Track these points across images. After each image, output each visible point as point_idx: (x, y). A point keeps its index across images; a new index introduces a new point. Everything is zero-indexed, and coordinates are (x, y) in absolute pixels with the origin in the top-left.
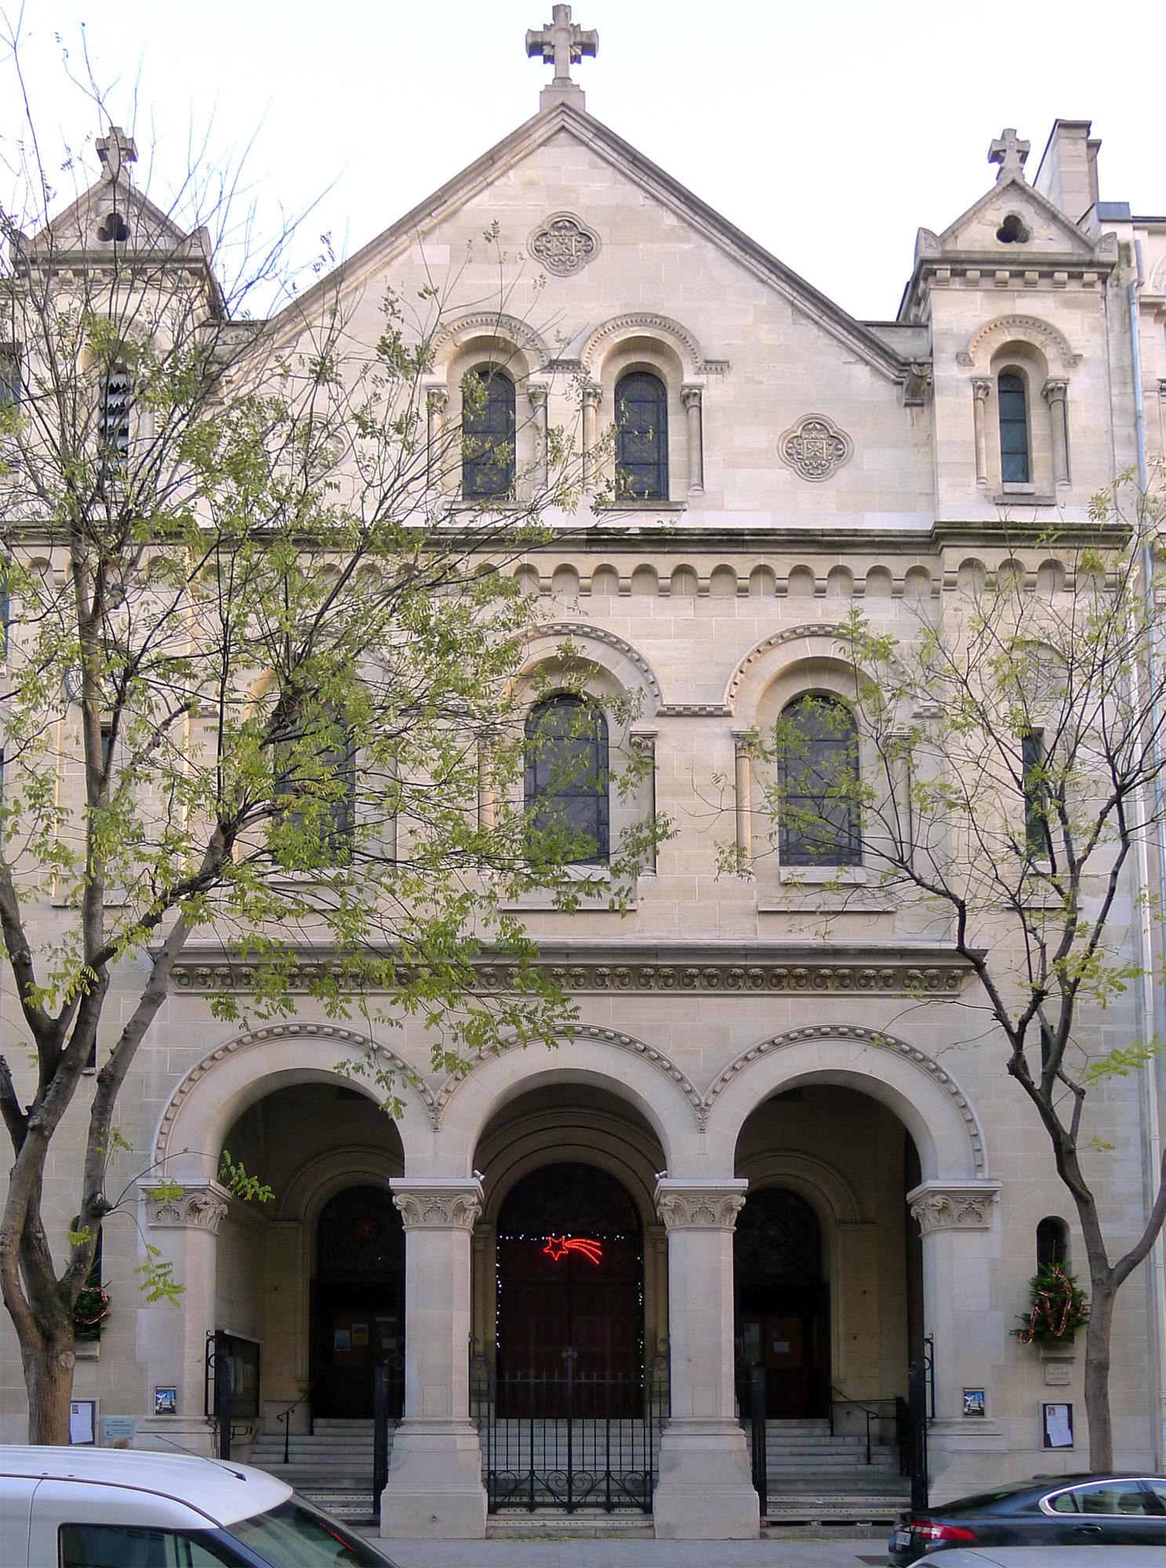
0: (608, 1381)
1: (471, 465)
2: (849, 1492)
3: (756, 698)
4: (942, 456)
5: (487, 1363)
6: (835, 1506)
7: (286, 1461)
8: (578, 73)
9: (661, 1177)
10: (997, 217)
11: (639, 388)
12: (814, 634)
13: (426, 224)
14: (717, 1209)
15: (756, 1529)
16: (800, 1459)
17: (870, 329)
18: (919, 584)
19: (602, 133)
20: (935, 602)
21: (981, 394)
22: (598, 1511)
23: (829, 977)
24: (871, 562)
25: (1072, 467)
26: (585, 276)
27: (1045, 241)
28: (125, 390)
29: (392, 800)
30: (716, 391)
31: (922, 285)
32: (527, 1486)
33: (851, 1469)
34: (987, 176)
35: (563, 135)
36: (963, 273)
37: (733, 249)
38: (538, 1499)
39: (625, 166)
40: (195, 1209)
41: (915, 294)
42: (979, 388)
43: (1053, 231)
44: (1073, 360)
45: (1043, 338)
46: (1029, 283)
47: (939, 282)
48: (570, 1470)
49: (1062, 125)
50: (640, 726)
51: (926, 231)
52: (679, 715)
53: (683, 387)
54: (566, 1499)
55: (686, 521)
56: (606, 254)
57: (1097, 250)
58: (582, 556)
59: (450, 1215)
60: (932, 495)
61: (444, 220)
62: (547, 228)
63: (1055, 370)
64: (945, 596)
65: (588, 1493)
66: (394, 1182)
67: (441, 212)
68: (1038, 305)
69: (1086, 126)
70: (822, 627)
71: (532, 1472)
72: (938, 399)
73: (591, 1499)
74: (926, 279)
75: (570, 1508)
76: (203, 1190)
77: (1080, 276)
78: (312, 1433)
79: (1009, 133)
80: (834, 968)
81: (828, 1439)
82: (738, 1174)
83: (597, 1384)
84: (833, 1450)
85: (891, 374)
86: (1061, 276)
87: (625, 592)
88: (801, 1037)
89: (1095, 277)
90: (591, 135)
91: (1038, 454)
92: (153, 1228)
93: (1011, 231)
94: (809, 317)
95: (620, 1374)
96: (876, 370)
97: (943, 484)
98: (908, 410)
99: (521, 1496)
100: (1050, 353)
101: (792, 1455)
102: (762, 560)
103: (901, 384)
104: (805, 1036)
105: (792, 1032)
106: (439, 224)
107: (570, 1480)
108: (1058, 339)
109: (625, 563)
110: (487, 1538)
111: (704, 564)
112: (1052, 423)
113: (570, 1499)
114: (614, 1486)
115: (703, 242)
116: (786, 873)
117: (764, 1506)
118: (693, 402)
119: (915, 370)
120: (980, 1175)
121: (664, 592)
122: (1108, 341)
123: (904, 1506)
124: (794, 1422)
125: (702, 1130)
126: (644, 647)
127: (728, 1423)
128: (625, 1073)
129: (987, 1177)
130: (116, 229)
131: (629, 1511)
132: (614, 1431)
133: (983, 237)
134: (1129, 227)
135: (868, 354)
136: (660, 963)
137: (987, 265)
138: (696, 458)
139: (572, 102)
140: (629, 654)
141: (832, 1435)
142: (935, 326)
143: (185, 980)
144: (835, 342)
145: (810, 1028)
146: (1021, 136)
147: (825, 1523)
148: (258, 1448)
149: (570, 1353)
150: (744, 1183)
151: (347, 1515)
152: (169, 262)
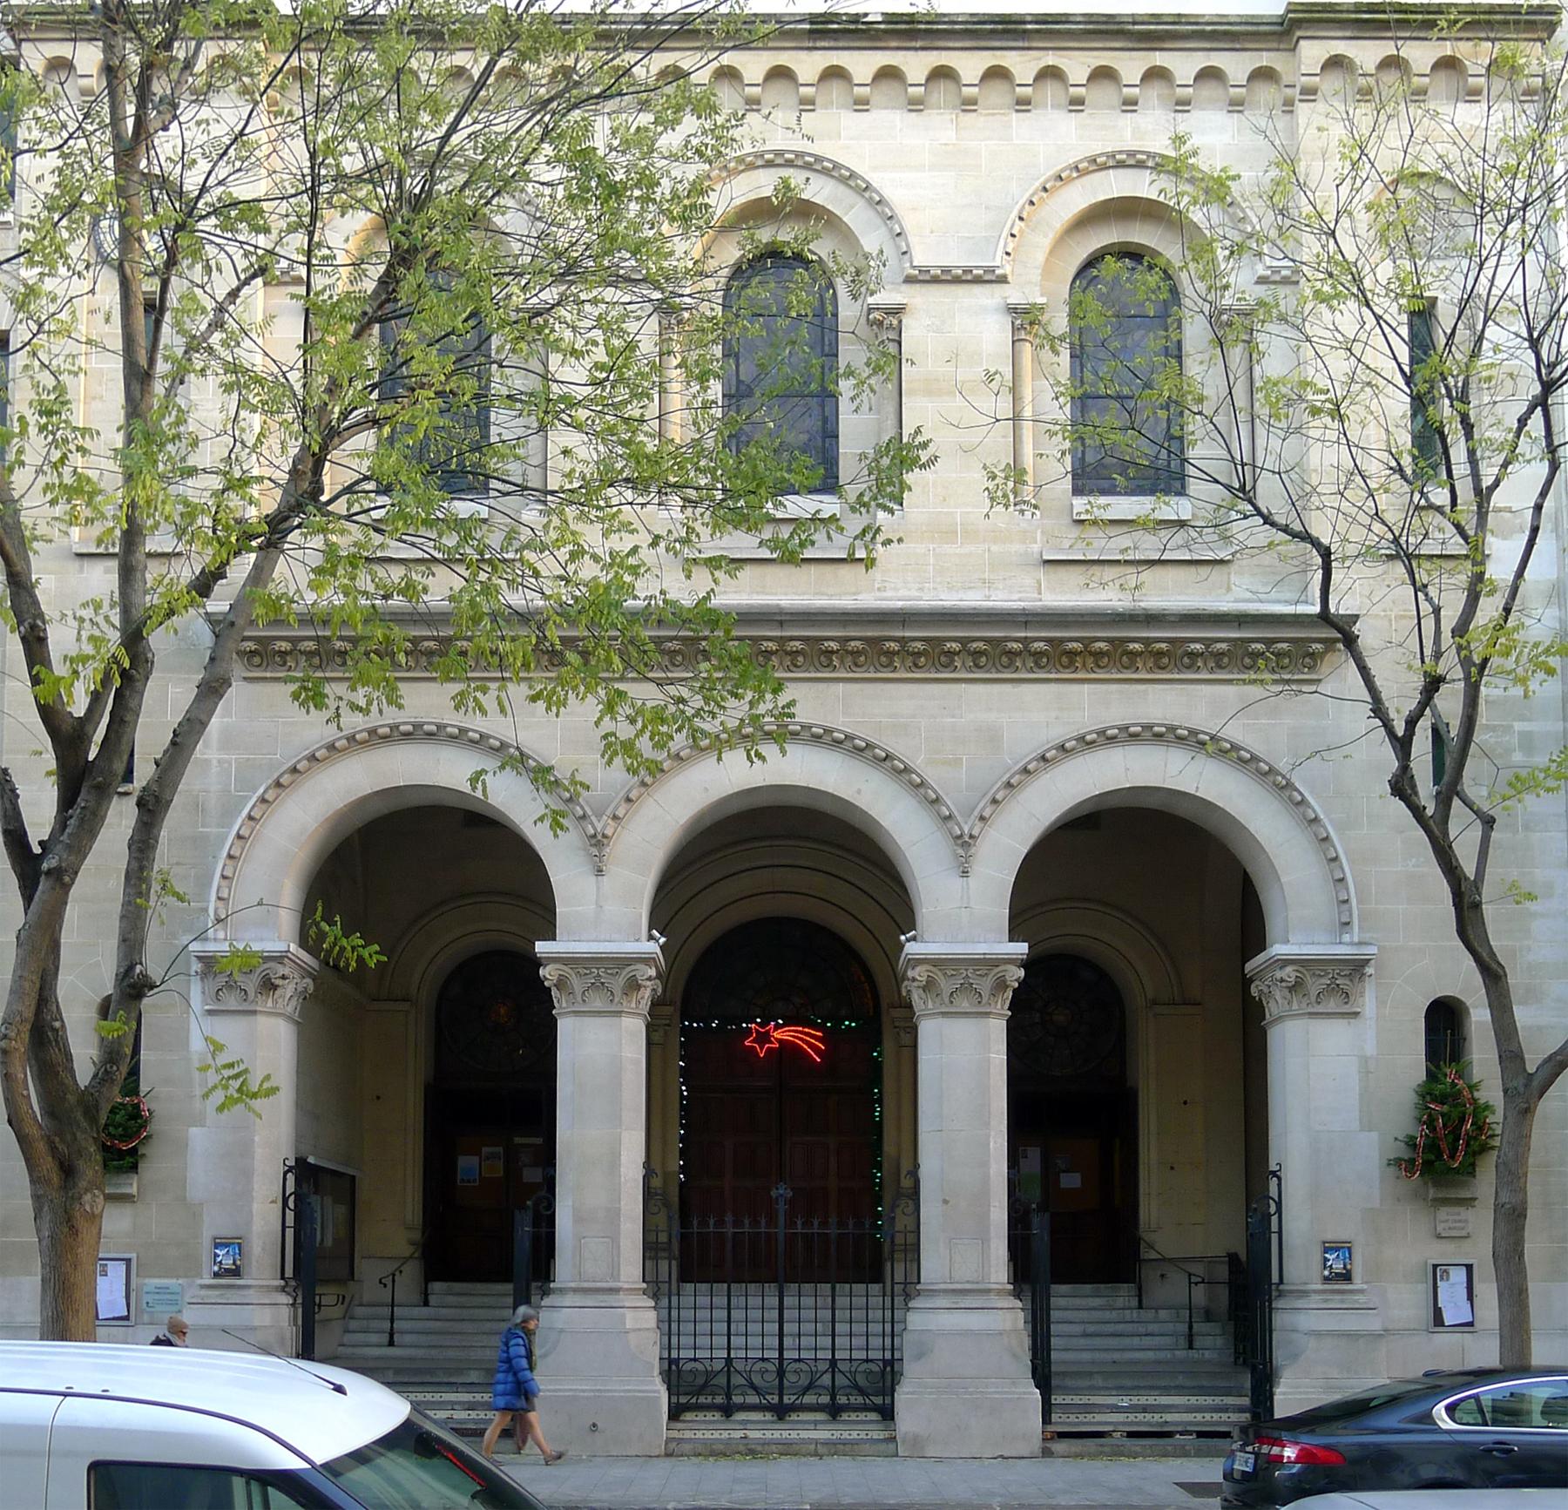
2: (1166, 1390)
3: (1040, 256)
5: (666, 1204)
6: (1145, 1409)
7: (391, 1343)
9: (908, 940)
14: (985, 985)
15: (1036, 1443)
18: (1266, 93)
24: (1200, 60)
32: (722, 1380)
38: (737, 1399)
40: (269, 986)
52: (935, 280)
54: (776, 1399)
58: (803, 55)
59: (618, 992)
64: (1303, 109)
65: (805, 1390)
66: (541, 947)
70: (1132, 154)
73: (809, 1399)
75: (781, 1412)
76: (280, 959)
78: (426, 1304)
80: (1147, 642)
84: (1142, 1329)
87: (861, 104)
92: (210, 1012)
99: (714, 1394)
101: (1085, 1335)
102: (1051, 59)
105: (1090, 733)
107: (781, 1373)
109: (862, 64)
113: (781, 1399)
120: (1346, 938)
121: (916, 105)
123: (1241, 1410)
126: (884, 183)
127: (999, 1292)
128: (859, 792)
129: (1356, 939)
132: (842, 1301)
140: (867, 195)
141: (1140, 1307)
143: (257, 660)
147: (1131, 1435)
148: (353, 1324)
149: (781, 1191)
150: (1022, 948)
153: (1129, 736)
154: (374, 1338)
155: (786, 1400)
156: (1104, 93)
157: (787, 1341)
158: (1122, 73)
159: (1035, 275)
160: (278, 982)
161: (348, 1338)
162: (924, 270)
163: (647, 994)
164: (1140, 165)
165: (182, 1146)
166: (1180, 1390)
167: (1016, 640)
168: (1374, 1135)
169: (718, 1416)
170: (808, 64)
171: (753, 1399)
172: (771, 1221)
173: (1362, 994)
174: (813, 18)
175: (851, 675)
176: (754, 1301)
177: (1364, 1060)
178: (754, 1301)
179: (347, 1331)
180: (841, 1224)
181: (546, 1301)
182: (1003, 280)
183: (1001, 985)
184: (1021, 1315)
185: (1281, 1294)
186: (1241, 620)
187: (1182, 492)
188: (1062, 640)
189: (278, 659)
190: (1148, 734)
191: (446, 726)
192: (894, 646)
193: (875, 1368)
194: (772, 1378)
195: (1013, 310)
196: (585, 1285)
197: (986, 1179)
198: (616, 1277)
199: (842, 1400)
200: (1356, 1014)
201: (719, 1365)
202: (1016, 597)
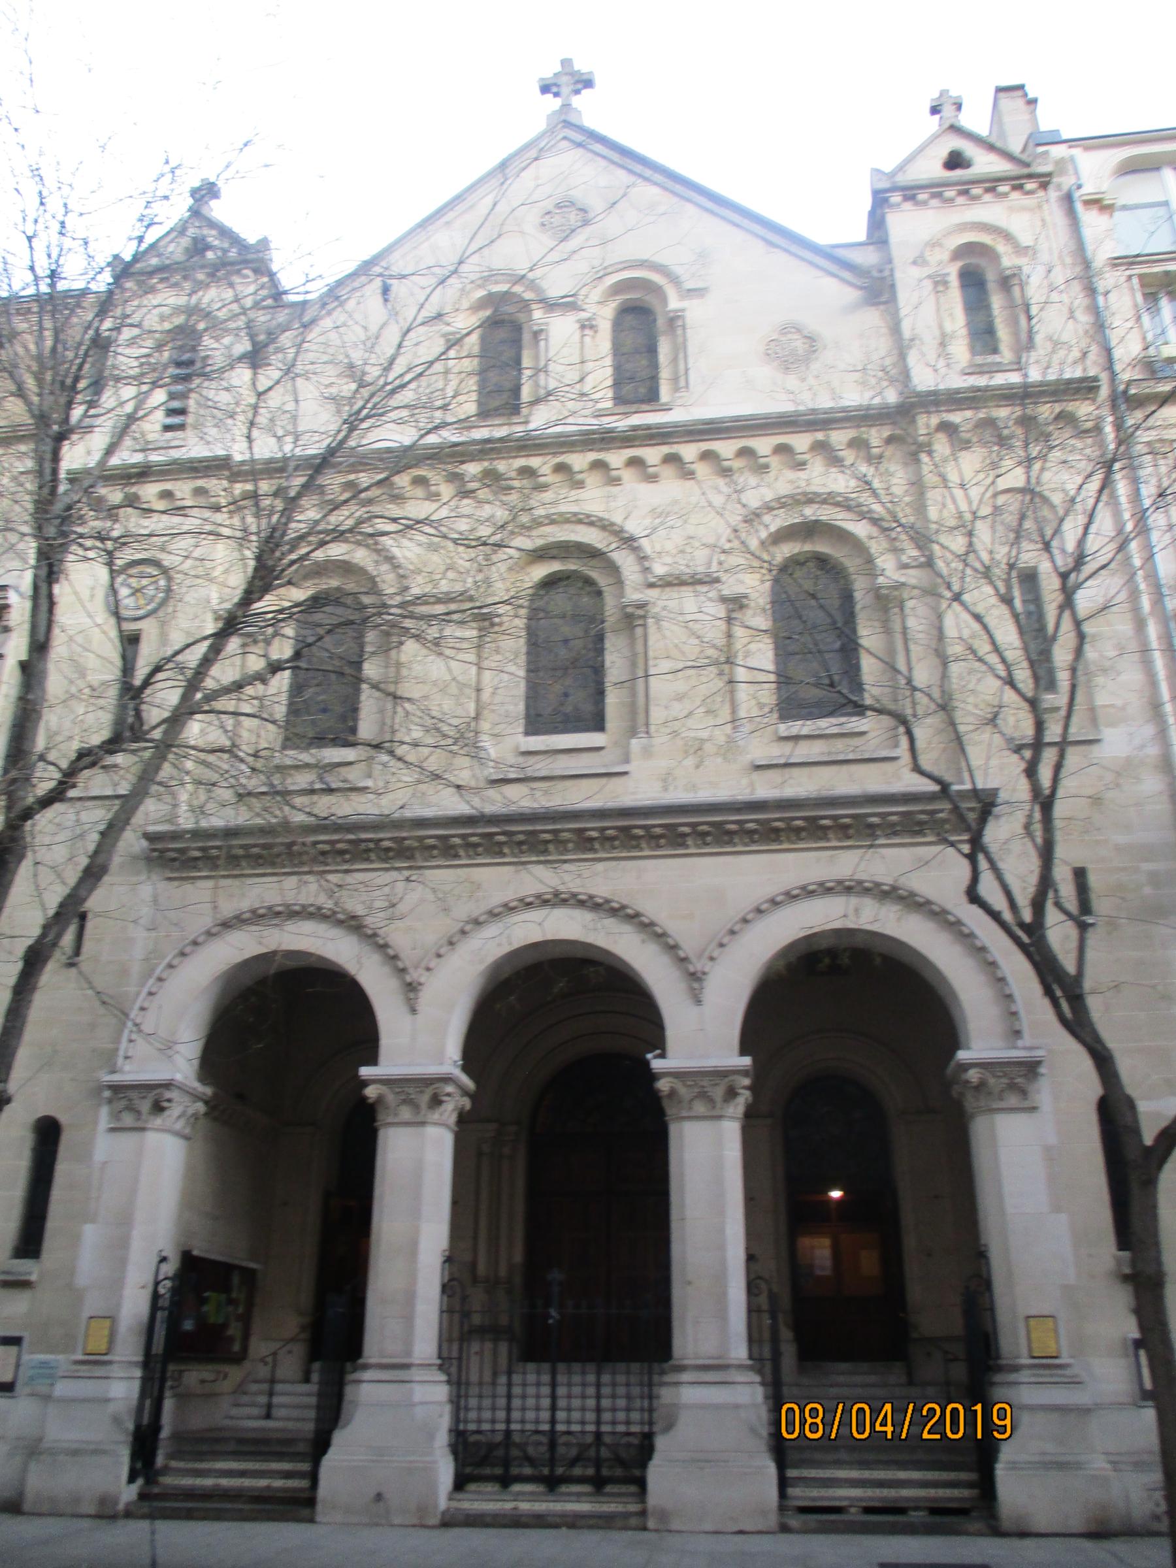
6: (881, 1484)
7: (268, 1416)
10: (942, 151)
11: (502, 334)
13: (450, 216)
15: (772, 1520)
22: (586, 1488)
23: (878, 825)
24: (592, 456)
27: (985, 163)
30: (695, 312)
31: (879, 212)
34: (933, 124)
37: (710, 205)
38: (515, 1471)
39: (615, 156)
41: (877, 223)
43: (992, 157)
46: (976, 198)
47: (891, 206)
49: (1000, 90)
51: (878, 170)
54: (546, 1471)
55: (676, 416)
65: (573, 1463)
66: (365, 1071)
67: (460, 208)
68: (990, 211)
69: (1021, 87)
73: (577, 1471)
76: (447, 1079)
79: (943, 93)
80: (835, 818)
82: (743, 1052)
88: (520, 904)
91: (1003, 333)
93: (955, 161)
99: (493, 1465)
100: (1001, 248)
104: (806, 893)
105: (513, 900)
107: (553, 1445)
108: (1007, 236)
110: (98, 1516)
113: (552, 1470)
114: (515, 1452)
117: (783, 1483)
119: (875, 274)
120: (1020, 1043)
123: (970, 1485)
124: (865, 1366)
127: (740, 1367)
131: (624, 1489)
132: (561, 1378)
133: (932, 168)
134: (1063, 147)
136: (558, 827)
137: (936, 189)
139: (573, 119)
145: (530, 896)
147: (868, 1510)
148: (245, 1399)
150: (747, 1061)
151: (935, 1500)
154: (255, 1411)
155: (560, 1471)
160: (165, 1104)
161: (234, 1411)
164: (592, 524)
165: (75, 1240)
168: (1063, 1217)
171: (528, 1471)
177: (1047, 1149)
179: (237, 1405)
181: (668, 1378)
185: (1000, 1369)
192: (640, 832)
193: (635, 1441)
195: (724, 600)
197: (723, 1263)
198: (409, 1353)
199: (605, 1472)
200: (1034, 1109)
201: (589, 1439)
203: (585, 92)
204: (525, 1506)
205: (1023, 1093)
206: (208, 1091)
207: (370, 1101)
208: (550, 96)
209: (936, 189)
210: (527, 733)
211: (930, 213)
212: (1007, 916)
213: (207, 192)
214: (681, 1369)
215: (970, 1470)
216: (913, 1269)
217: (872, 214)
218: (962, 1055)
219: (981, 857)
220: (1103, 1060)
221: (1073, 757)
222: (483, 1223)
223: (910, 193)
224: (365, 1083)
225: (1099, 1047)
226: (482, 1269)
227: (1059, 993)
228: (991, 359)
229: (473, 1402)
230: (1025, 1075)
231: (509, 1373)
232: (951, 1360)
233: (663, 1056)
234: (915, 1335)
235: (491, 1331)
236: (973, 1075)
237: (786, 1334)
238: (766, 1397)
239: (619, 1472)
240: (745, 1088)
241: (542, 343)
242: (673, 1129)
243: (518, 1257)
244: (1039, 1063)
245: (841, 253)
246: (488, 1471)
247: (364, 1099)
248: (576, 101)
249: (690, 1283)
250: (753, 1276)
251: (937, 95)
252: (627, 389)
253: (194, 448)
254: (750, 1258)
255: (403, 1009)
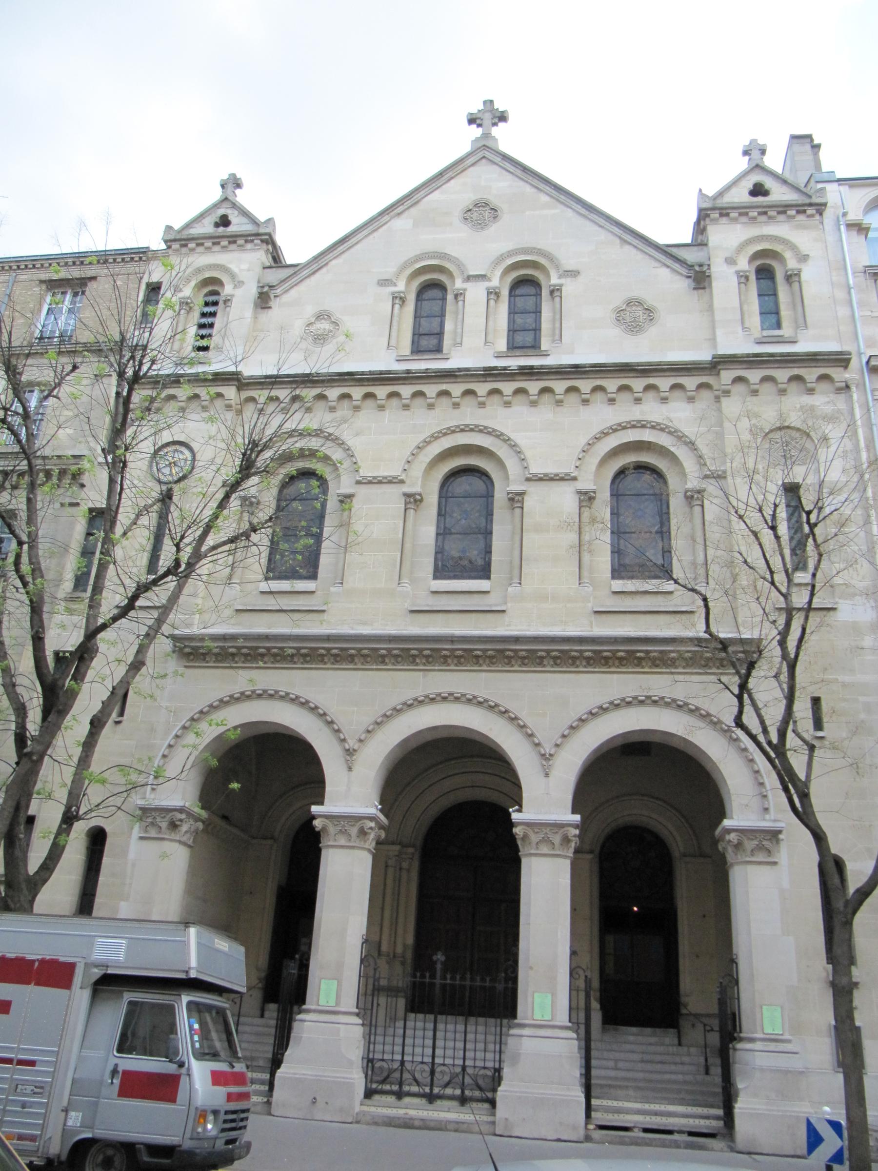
0: (468, 983)
1: (418, 335)
3: (593, 467)
4: (718, 316)
5: (403, 963)
6: (656, 1114)
8: (495, 131)
9: (514, 811)
10: (748, 184)
12: (634, 427)
14: (557, 839)
15: (582, 1133)
16: (649, 1067)
17: (670, 248)
18: (705, 394)
19: (506, 157)
20: (718, 405)
21: (743, 280)
25: (808, 318)
26: (493, 229)
27: (779, 194)
28: (215, 304)
29: (171, 475)
30: (570, 288)
31: (702, 223)
32: (397, 1075)
33: (689, 1078)
35: (484, 161)
36: (727, 215)
37: (583, 211)
38: (406, 1088)
39: (519, 172)
40: (174, 826)
41: (700, 229)
42: (742, 276)
43: (785, 189)
44: (804, 258)
45: (782, 247)
46: (770, 218)
47: (712, 220)
48: (433, 1063)
49: (794, 138)
50: (515, 487)
52: (541, 479)
53: (550, 286)
54: (427, 1090)
55: (452, 364)
56: (506, 218)
57: (813, 197)
60: (713, 340)
61: (411, 206)
62: (471, 207)
63: (792, 264)
64: (723, 399)
65: (446, 1085)
66: (315, 809)
68: (780, 229)
69: (809, 137)
70: (639, 421)
71: (402, 1062)
72: (714, 284)
73: (449, 1091)
74: (704, 220)
75: (431, 1098)
77: (804, 212)
78: (262, 1016)
79: (753, 142)
80: (647, 652)
81: (675, 1049)
82: (574, 812)
83: (450, 984)
84: (678, 1060)
85: (684, 271)
86: (792, 212)
87: (508, 404)
89: (814, 212)
90: (499, 159)
91: (785, 313)
92: (141, 838)
93: (758, 190)
94: (630, 244)
95: (448, 976)
96: (674, 271)
97: (719, 332)
98: (695, 292)
99: (391, 1084)
100: (788, 255)
101: (642, 1061)
102: (599, 382)
103: (690, 277)
105: (616, 700)
106: (408, 208)
107: (432, 1073)
108: (793, 247)
109: (508, 388)
111: (559, 386)
112: (793, 294)
113: (431, 1089)
115: (565, 208)
116: (618, 585)
118: (557, 294)
119: (697, 268)
120: (767, 817)
121: (534, 404)
122: (826, 247)
123: (717, 1118)
124: (649, 1030)
125: (547, 775)
126: (518, 438)
128: (491, 729)
129: (772, 818)
130: (224, 222)
132: (441, 1026)
133: (741, 195)
135: (669, 262)
137: (743, 211)
138: (557, 325)
139: (490, 143)
141: (680, 1044)
142: (710, 244)
143: (192, 657)
144: (647, 257)
146: (761, 142)
147: (646, 1130)
149: (440, 957)
150: (577, 817)
152: (248, 237)
153: (244, 697)
155: (436, 1090)
156: (625, 396)
157: (439, 1052)
158: (427, 393)
159: (591, 477)
162: (535, 475)
163: (573, 845)
166: (682, 1102)
167: (576, 651)
169: (424, 1101)
170: (482, 389)
171: (415, 1089)
172: (433, 976)
173: (779, 852)
174: (485, 369)
175: (552, 669)
176: (451, 1027)
178: (451, 1027)
180: (472, 979)
181: (513, 1031)
182: (402, 482)
183: (566, 840)
184: (576, 1042)
185: (741, 1040)
186: (581, 640)
187: (488, 577)
188: (601, 651)
189: (603, 661)
190: (635, 702)
191: (279, 691)
193: (489, 1073)
194: (427, 1074)
196: (320, 1008)
200: (775, 863)
202: (579, 629)
203: (500, 124)
204: (412, 1113)
205: (769, 852)
206: (204, 814)
207: (317, 829)
208: (474, 126)
209: (743, 211)
210: (435, 577)
211: (739, 226)
212: (761, 738)
213: (234, 183)
214: (522, 1026)
215: (719, 1108)
216: (685, 964)
217: (698, 223)
218: (726, 823)
219: (746, 696)
220: (819, 838)
221: (814, 618)
222: (387, 914)
223: (724, 212)
224: (314, 818)
225: (818, 831)
226: (384, 948)
227: (792, 791)
228: (777, 332)
229: (380, 1039)
230: (770, 839)
231: (373, 995)
232: (708, 1031)
233: (520, 811)
234: (684, 1011)
235: (391, 991)
236: (733, 837)
237: (595, 1005)
238: (579, 1048)
239: (477, 1094)
240: (575, 836)
241: (460, 303)
242: (524, 862)
243: (410, 940)
244: (780, 832)
245: (674, 251)
246: (387, 1087)
247: (313, 828)
248: (495, 131)
249: (531, 968)
250: (574, 966)
251: (747, 143)
252: (519, 338)
253: (217, 364)
254: (573, 953)
255: (344, 768)
